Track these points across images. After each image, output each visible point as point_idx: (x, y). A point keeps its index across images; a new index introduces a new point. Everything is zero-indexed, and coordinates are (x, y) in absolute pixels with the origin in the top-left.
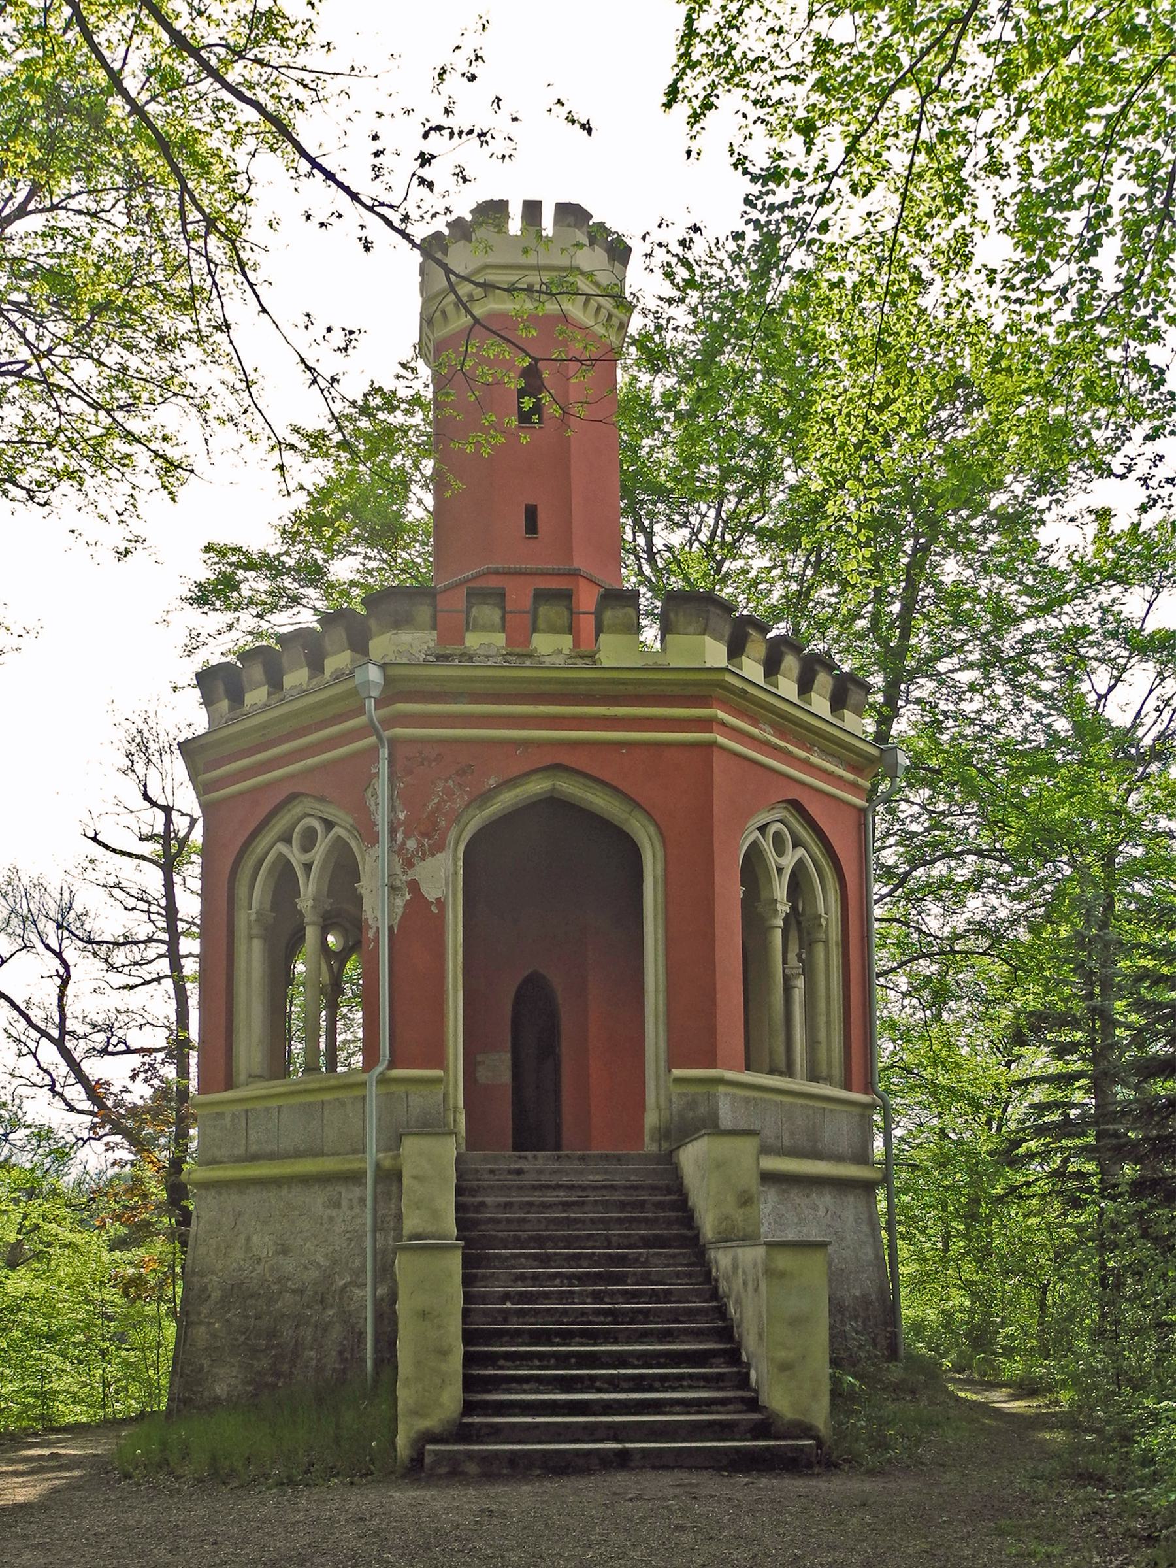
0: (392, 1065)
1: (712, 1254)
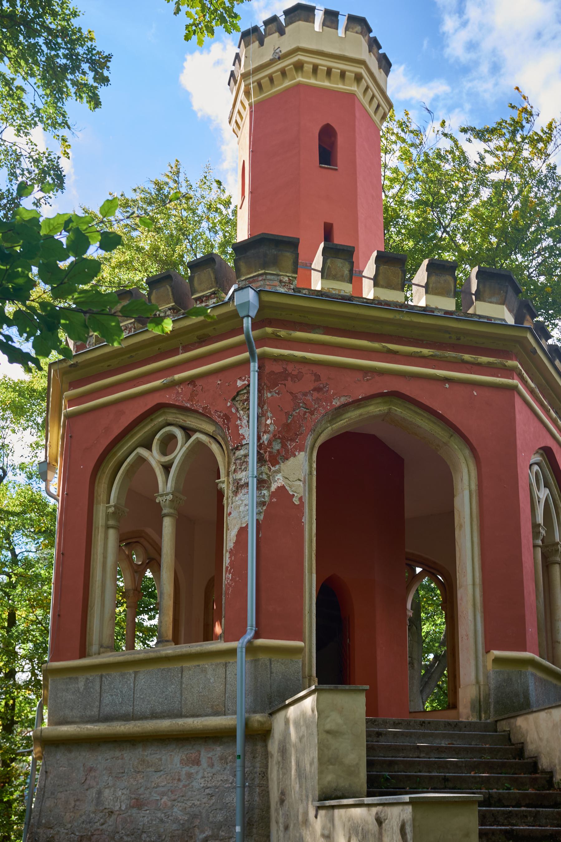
0: (257, 636)
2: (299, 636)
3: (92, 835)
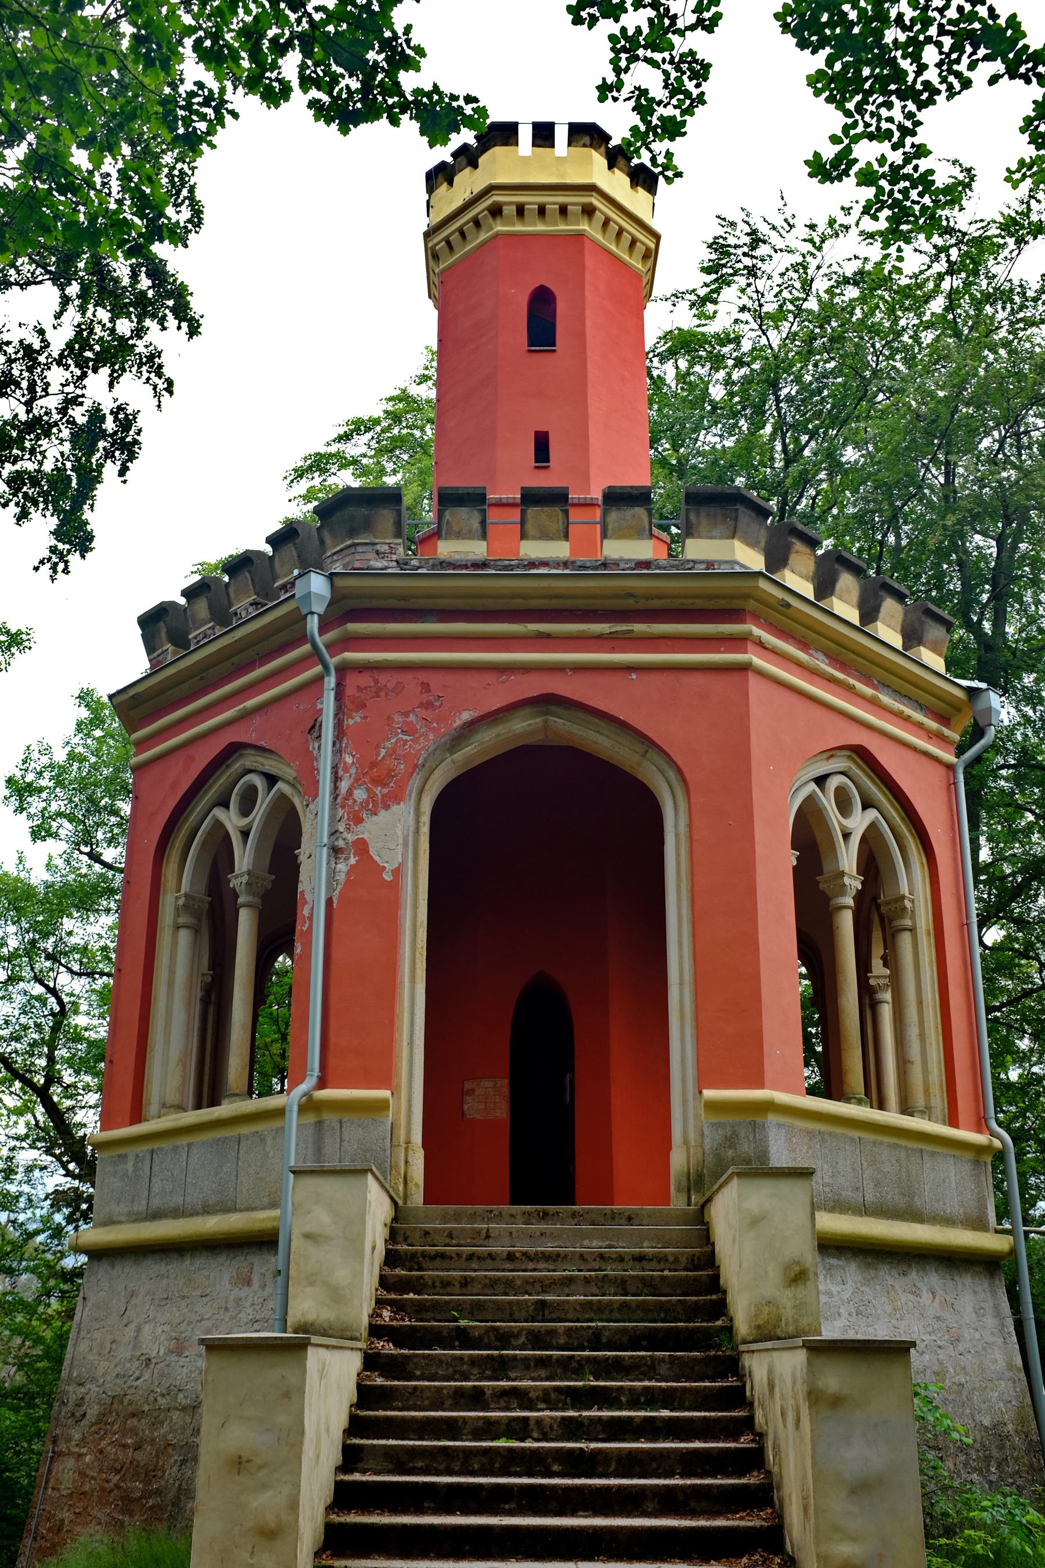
1: (747, 1361)
2: (384, 1077)
3: (125, 1395)
